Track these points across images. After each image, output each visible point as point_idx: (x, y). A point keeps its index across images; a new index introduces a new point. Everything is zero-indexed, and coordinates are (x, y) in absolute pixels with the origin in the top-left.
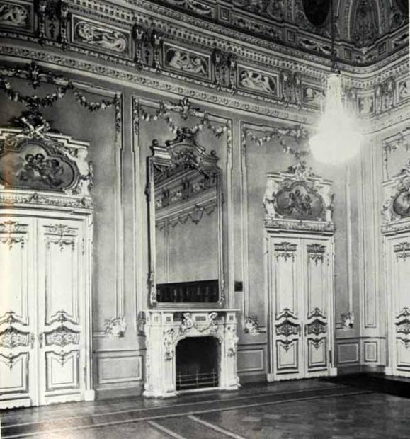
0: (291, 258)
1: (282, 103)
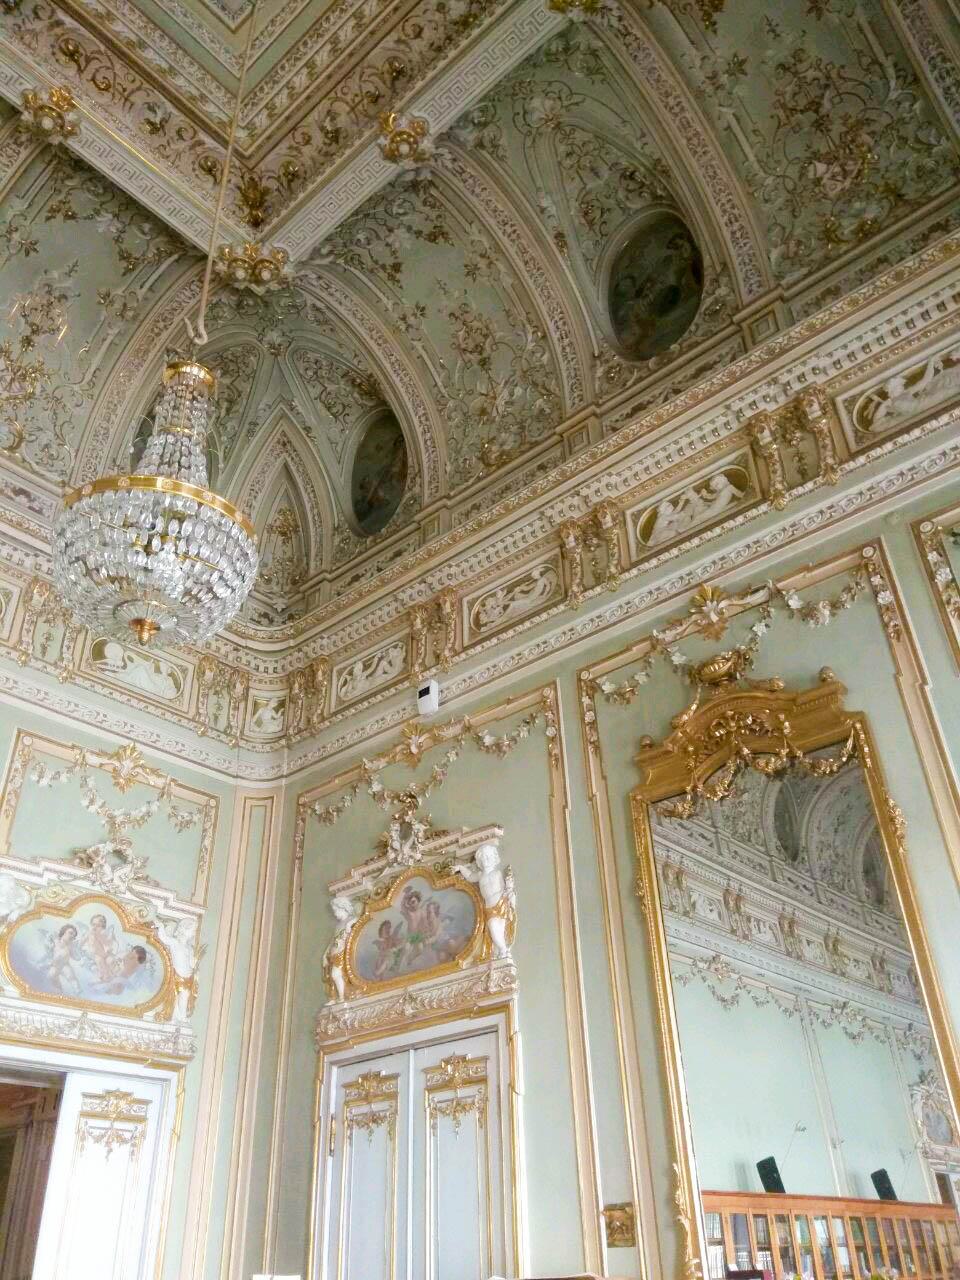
0: (127, 1148)
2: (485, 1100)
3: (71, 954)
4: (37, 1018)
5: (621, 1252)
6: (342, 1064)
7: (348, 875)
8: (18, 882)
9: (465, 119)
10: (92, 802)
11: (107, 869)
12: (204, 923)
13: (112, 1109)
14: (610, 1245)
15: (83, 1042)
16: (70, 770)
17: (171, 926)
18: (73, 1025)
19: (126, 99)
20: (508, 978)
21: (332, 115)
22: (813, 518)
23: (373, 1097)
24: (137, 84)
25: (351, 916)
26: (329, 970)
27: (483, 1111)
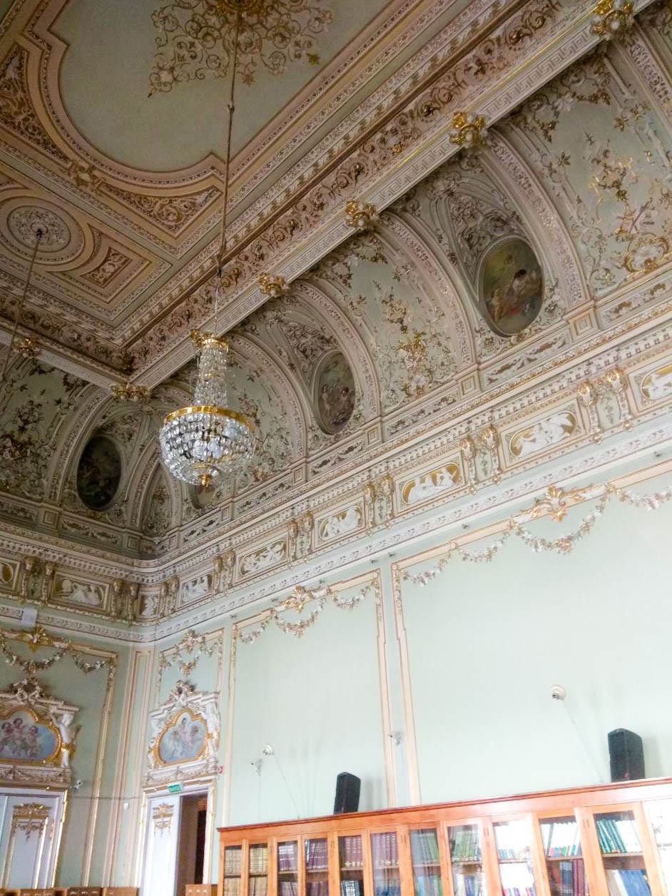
1: (107, 618)
19: (554, 7)
24: (451, 75)
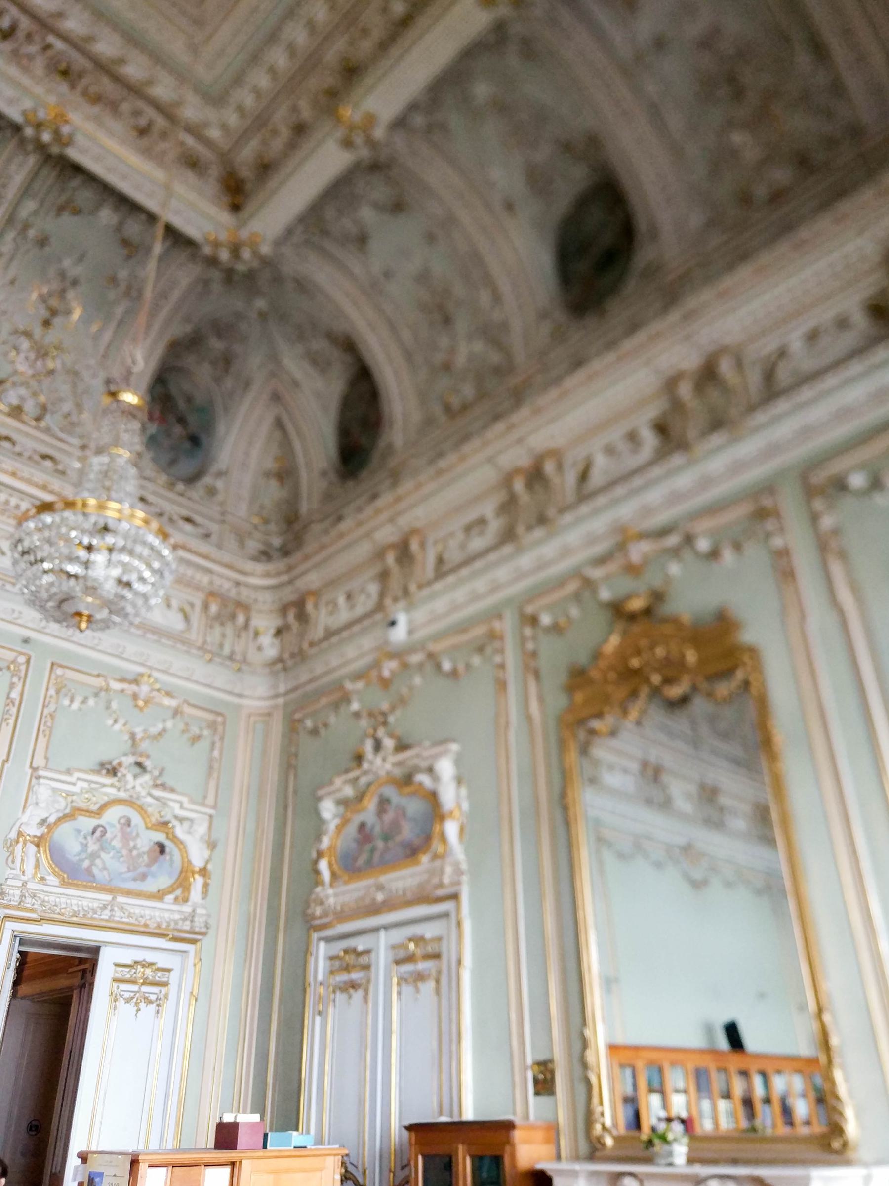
0: (153, 1007)
2: (439, 972)
3: (102, 849)
4: (74, 902)
5: (544, 1099)
6: (328, 940)
7: (331, 783)
8: (54, 790)
9: (413, 107)
10: (116, 721)
11: (130, 777)
12: (216, 824)
13: (139, 975)
14: (537, 1093)
15: (113, 921)
16: (96, 695)
17: (186, 824)
18: (104, 907)
20: (458, 872)
21: (295, 109)
22: (724, 465)
23: (352, 966)
25: (335, 816)
26: (316, 862)
27: (438, 982)
